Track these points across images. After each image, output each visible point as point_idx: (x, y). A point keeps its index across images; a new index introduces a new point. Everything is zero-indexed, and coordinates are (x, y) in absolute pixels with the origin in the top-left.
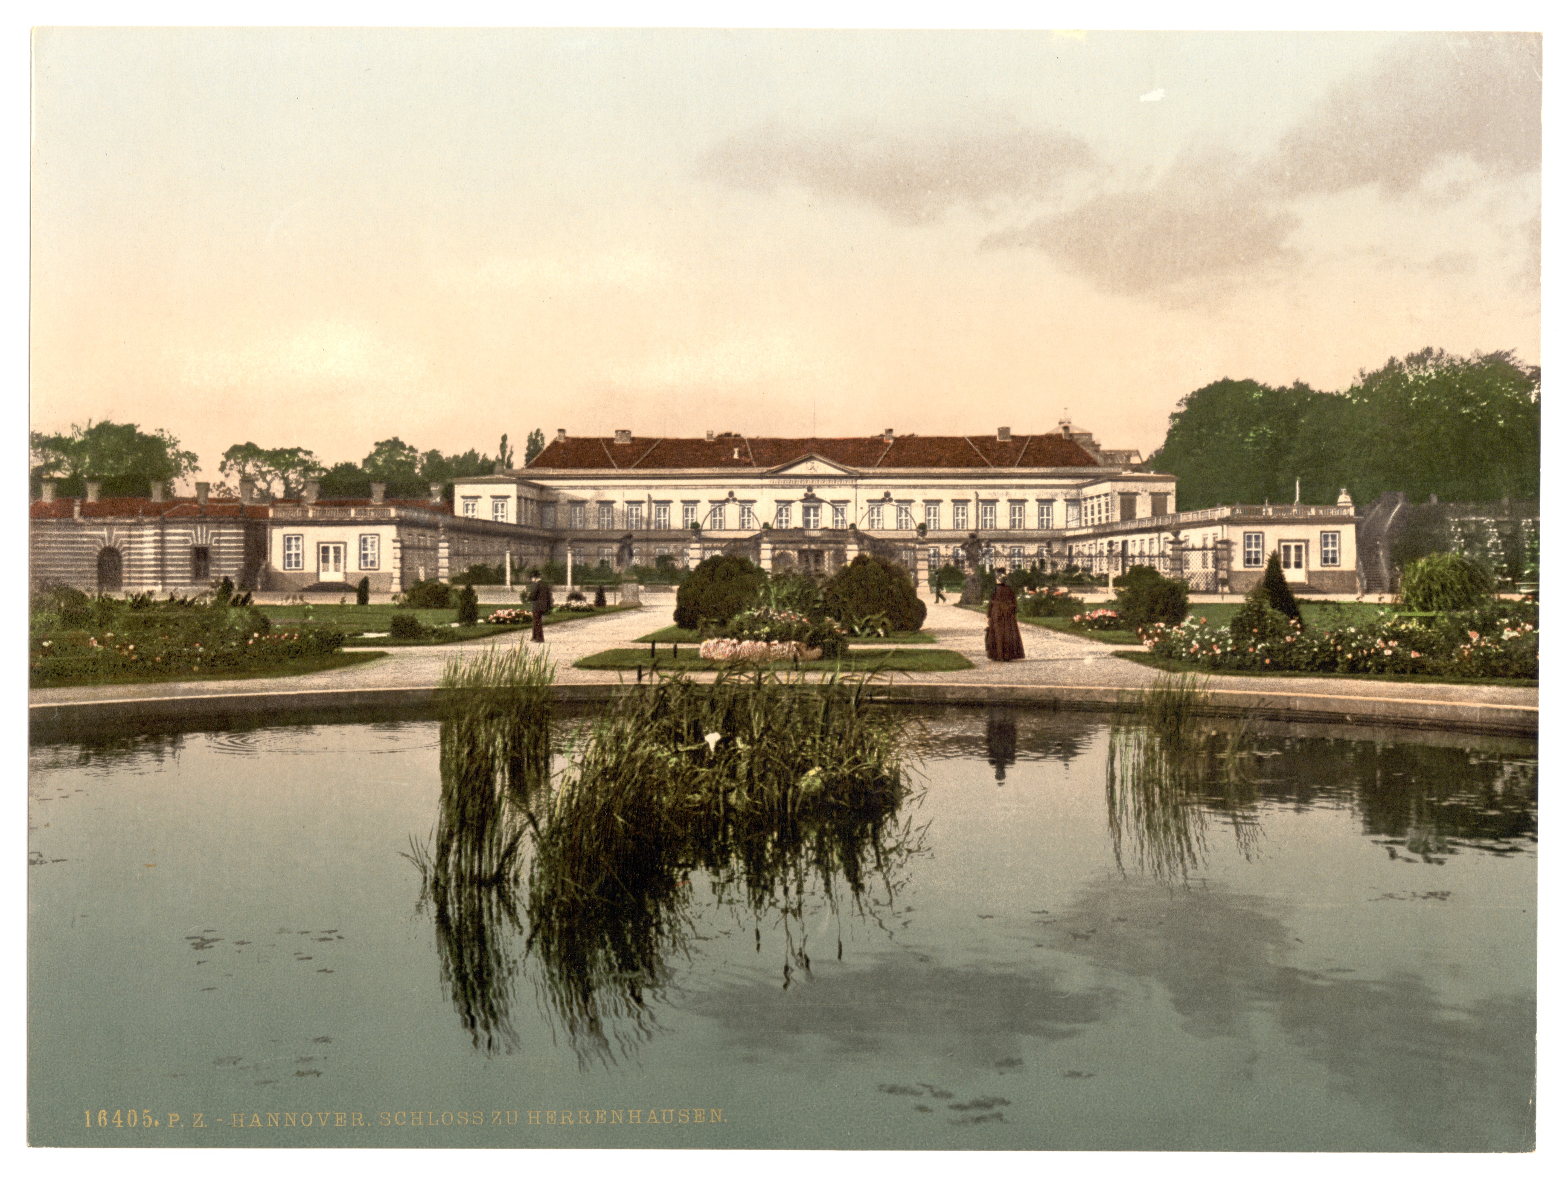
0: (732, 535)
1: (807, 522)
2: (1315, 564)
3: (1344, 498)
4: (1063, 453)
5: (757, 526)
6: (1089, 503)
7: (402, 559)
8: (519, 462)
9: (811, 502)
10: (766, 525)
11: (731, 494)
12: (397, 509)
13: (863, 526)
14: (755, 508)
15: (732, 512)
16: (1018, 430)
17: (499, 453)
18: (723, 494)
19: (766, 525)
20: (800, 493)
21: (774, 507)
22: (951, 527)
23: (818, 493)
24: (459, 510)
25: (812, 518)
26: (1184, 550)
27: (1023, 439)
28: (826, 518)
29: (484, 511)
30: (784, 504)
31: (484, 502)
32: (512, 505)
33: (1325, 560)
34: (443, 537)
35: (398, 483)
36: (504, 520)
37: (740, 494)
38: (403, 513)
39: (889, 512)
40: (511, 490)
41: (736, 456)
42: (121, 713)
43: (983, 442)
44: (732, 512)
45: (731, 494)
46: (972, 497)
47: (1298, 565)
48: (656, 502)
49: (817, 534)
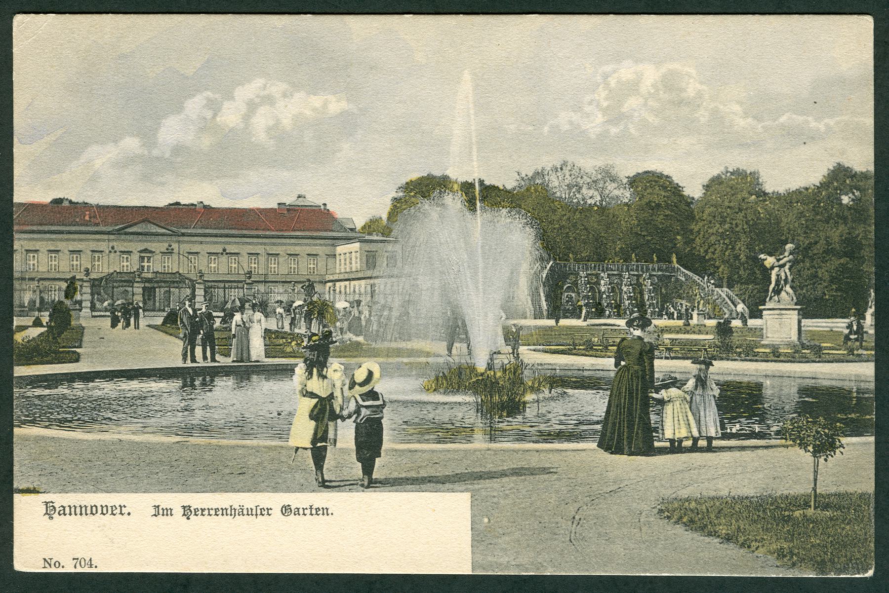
11: (224, 250)
18: (218, 249)
45: (224, 250)
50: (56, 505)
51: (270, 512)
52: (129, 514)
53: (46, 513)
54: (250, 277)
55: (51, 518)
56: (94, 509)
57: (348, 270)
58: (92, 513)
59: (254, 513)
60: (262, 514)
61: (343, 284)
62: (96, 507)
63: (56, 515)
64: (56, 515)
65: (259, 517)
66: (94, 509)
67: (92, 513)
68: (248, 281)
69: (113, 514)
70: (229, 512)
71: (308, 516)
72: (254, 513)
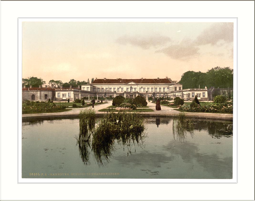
0: (120, 93)
1: (131, 91)
4: (166, 81)
5: (124, 91)
6: (170, 88)
8: (90, 82)
10: (125, 91)
13: (139, 91)
14: (123, 89)
18: (119, 87)
19: (125, 91)
20: (130, 87)
21: (126, 89)
23: (132, 87)
24: (82, 89)
25: (131, 90)
29: (85, 89)
32: (89, 88)
38: (74, 90)
40: (89, 86)
41: (121, 82)
45: (120, 87)
47: (199, 97)
49: (132, 92)
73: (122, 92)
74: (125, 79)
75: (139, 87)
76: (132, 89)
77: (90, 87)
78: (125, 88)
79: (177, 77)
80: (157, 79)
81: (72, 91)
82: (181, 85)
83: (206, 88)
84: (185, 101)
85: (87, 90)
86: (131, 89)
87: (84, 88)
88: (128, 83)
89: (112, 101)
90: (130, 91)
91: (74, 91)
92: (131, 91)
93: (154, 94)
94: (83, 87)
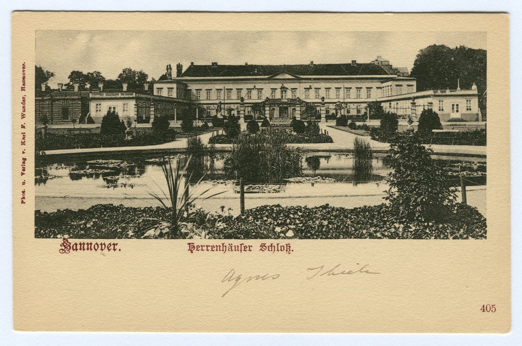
0: (254, 101)
1: (282, 96)
2: (464, 111)
3: (474, 87)
4: (375, 70)
5: (263, 99)
6: (385, 89)
7: (138, 111)
8: (174, 74)
9: (284, 89)
10: (267, 98)
11: (255, 87)
12: (136, 93)
13: (303, 98)
14: (263, 91)
15: (254, 93)
16: (316, 63)
17: (166, 71)
18: (252, 87)
19: (267, 98)
20: (280, 85)
21: (270, 91)
22: (216, 99)
23: (286, 85)
24: (155, 93)
25: (284, 95)
26: (416, 106)
27: (361, 65)
28: (289, 95)
29: (165, 93)
30: (274, 90)
31: (166, 91)
32: (175, 90)
33: (467, 109)
34: (152, 103)
35: (133, 83)
36: (172, 97)
37: (258, 86)
38: (137, 95)
39: (312, 92)
40: (174, 86)
41: (256, 72)
42: (204, 233)
43: (347, 66)
44: (254, 93)
45: (255, 87)
46: (342, 87)
47: (457, 111)
48: (346, 88)
49: (286, 101)
50: (195, 245)
51: (251, 248)
52: (120, 250)
53: (189, 250)
54: (323, 101)
55: (192, 252)
56: (282, 248)
57: (390, 95)
58: (281, 250)
59: (239, 249)
60: (245, 250)
61: (395, 102)
62: (284, 247)
63: (71, 250)
64: (194, 251)
65: (243, 252)
66: (282, 248)
67: (281, 250)
68: (323, 103)
69: (197, 250)
70: (221, 249)
71: (205, 251)
72: (239, 249)
73: (259, 98)
74: (508, 94)
75: (301, 87)
76: (285, 91)
77: (177, 88)
78: (267, 90)
79: (406, 62)
80: (350, 64)
81: (133, 98)
82: (414, 80)
83: (474, 87)
84: (305, 169)
85: (167, 96)
86: (282, 92)
87: (249, 90)
88: (278, 75)
89: (201, 136)
90: (280, 97)
91: (137, 99)
92: (282, 96)
93: (339, 106)
94: (157, 88)
